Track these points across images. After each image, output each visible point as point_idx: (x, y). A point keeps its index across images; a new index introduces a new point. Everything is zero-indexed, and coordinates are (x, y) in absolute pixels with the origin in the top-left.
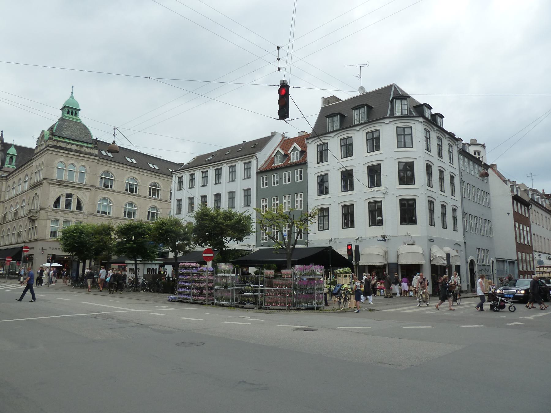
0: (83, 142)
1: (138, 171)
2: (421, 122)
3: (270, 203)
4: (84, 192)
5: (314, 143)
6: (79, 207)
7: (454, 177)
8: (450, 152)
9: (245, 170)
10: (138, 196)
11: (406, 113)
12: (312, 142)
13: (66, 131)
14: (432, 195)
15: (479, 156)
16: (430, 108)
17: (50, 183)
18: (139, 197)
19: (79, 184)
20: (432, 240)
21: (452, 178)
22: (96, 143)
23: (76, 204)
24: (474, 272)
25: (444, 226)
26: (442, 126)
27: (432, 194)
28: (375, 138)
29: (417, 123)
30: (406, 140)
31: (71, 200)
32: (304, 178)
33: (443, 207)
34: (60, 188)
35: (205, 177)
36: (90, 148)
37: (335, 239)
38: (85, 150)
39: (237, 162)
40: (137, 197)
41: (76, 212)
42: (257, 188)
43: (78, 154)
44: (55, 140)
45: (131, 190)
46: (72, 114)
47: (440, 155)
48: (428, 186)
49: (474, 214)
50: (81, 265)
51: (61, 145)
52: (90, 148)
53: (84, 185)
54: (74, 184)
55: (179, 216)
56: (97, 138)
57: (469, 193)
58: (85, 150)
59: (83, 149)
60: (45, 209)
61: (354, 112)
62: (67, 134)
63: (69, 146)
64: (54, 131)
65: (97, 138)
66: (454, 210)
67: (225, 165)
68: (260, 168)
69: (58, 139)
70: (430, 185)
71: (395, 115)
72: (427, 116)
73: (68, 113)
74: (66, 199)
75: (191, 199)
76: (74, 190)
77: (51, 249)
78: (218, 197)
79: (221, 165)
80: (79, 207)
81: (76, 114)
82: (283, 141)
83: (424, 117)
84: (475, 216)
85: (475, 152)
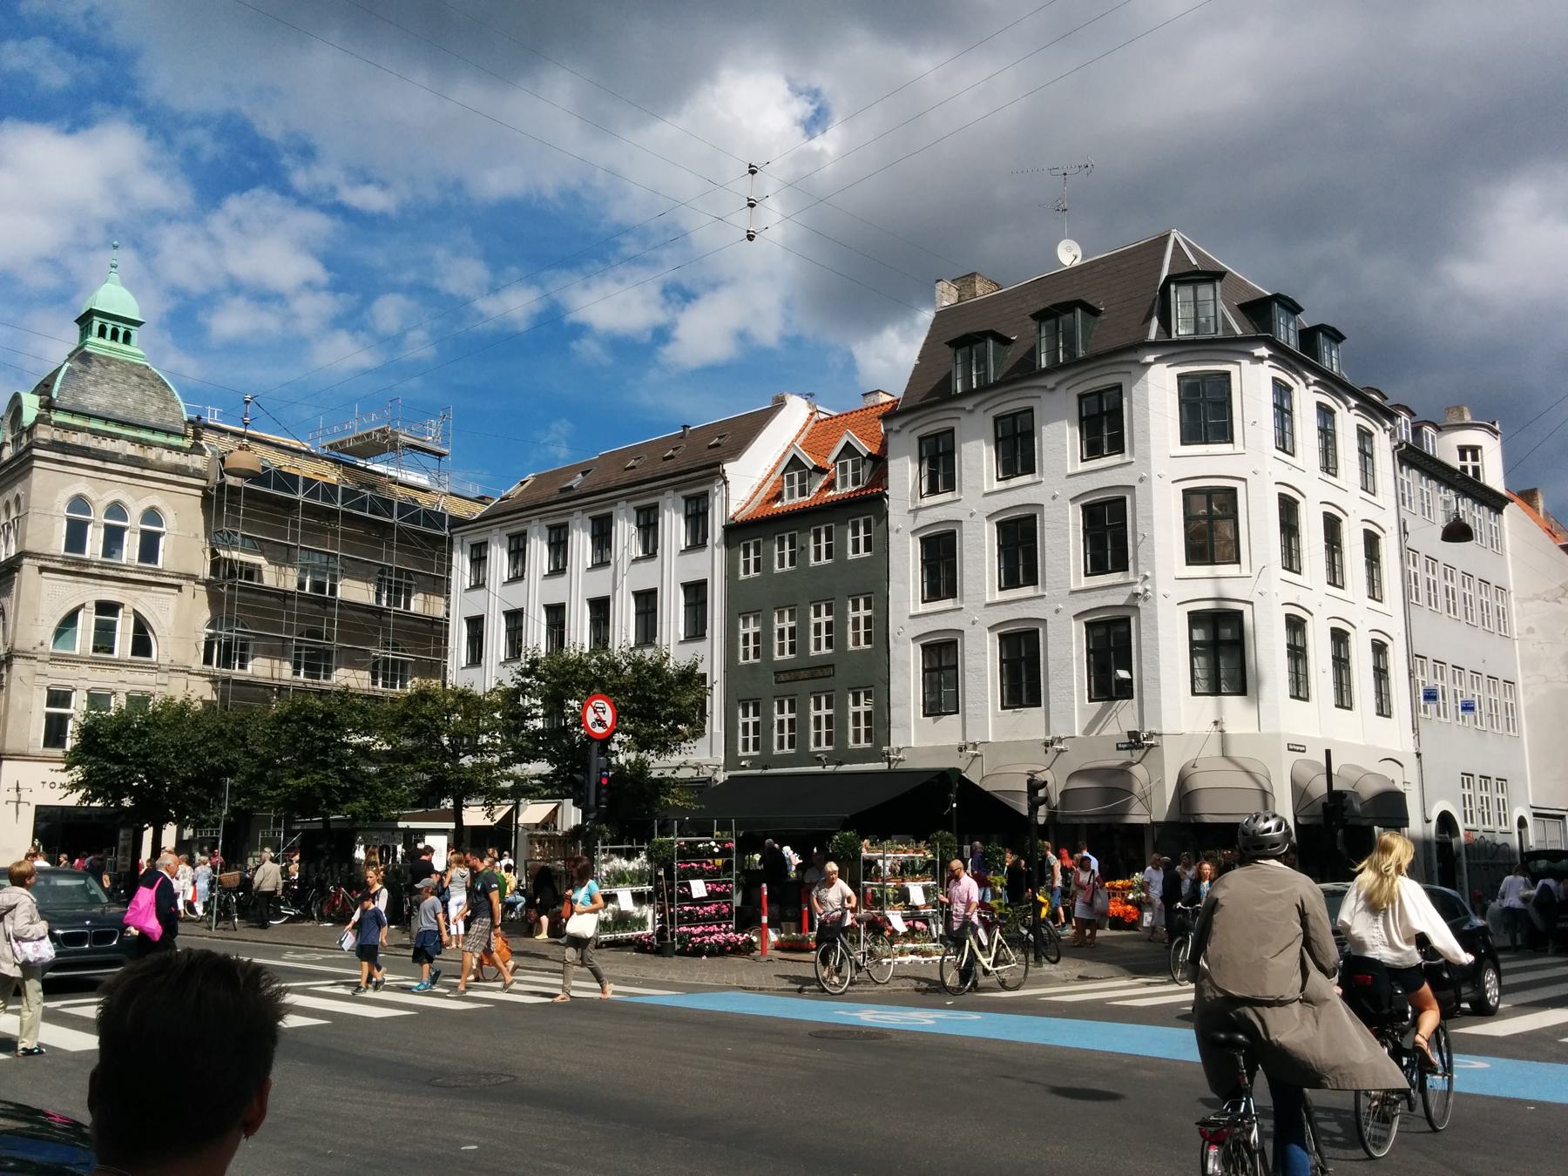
0: (153, 430)
3: (768, 626)
4: (157, 595)
5: (911, 432)
6: (142, 644)
7: (1378, 537)
8: (1366, 455)
9: (689, 520)
12: (902, 427)
15: (1476, 464)
16: (1293, 308)
17: (42, 569)
20: (1298, 748)
21: (1371, 541)
23: (131, 637)
25: (1343, 699)
28: (1019, 435)
31: (115, 622)
32: (878, 545)
33: (1339, 637)
34: (77, 582)
35: (559, 546)
36: (178, 449)
38: (159, 457)
41: (130, 661)
43: (137, 471)
44: (59, 425)
47: (1329, 463)
48: (1284, 568)
50: (148, 835)
51: (77, 439)
52: (178, 449)
55: (474, 673)
59: (152, 454)
60: (28, 652)
63: (107, 445)
64: (54, 395)
66: (1379, 649)
67: (622, 504)
68: (736, 514)
69: (67, 419)
70: (1291, 564)
71: (1174, 336)
72: (1282, 338)
74: (97, 620)
75: (514, 618)
76: (123, 588)
77: (47, 785)
78: (600, 608)
79: (657, 494)
80: (142, 644)
81: (127, 338)
82: (811, 424)
83: (1272, 343)
84: (1434, 661)
85: (1463, 450)
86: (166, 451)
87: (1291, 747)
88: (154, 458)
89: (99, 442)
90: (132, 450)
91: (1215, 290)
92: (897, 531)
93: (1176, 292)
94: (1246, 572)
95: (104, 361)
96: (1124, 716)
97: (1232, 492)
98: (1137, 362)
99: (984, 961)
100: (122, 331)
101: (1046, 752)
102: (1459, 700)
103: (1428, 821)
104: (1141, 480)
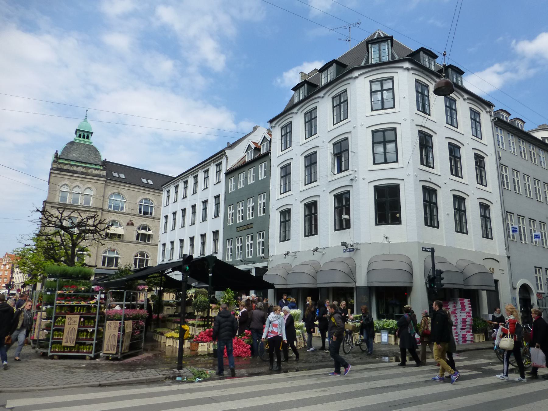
0: (91, 164)
1: (154, 192)
2: (407, 69)
7: (483, 158)
10: (153, 218)
11: (385, 59)
13: (73, 153)
14: (431, 179)
18: (154, 220)
19: (84, 207)
22: (104, 165)
24: (532, 304)
26: (460, 84)
27: (430, 177)
29: (400, 71)
30: (385, 97)
36: (98, 169)
37: (296, 253)
39: (210, 165)
40: (152, 220)
42: (225, 193)
43: (84, 176)
45: (146, 213)
46: (84, 137)
49: (516, 212)
51: (66, 167)
52: (98, 169)
53: (89, 207)
54: (79, 207)
56: (106, 159)
57: (539, 192)
58: (92, 171)
61: (322, 75)
62: (74, 157)
63: (75, 169)
65: (106, 159)
69: (64, 161)
73: (80, 136)
81: (88, 138)
84: (529, 218)
86: (94, 170)
87: (424, 249)
88: (90, 172)
89: (73, 168)
90: (83, 170)
91: (388, 44)
92: (274, 166)
93: (371, 48)
94: (401, 166)
95: (78, 144)
96: (346, 236)
97: (395, 129)
98: (351, 78)
99: (236, 352)
100: (86, 135)
101: (314, 254)
102: (533, 234)
103: (515, 289)
104: (354, 128)
